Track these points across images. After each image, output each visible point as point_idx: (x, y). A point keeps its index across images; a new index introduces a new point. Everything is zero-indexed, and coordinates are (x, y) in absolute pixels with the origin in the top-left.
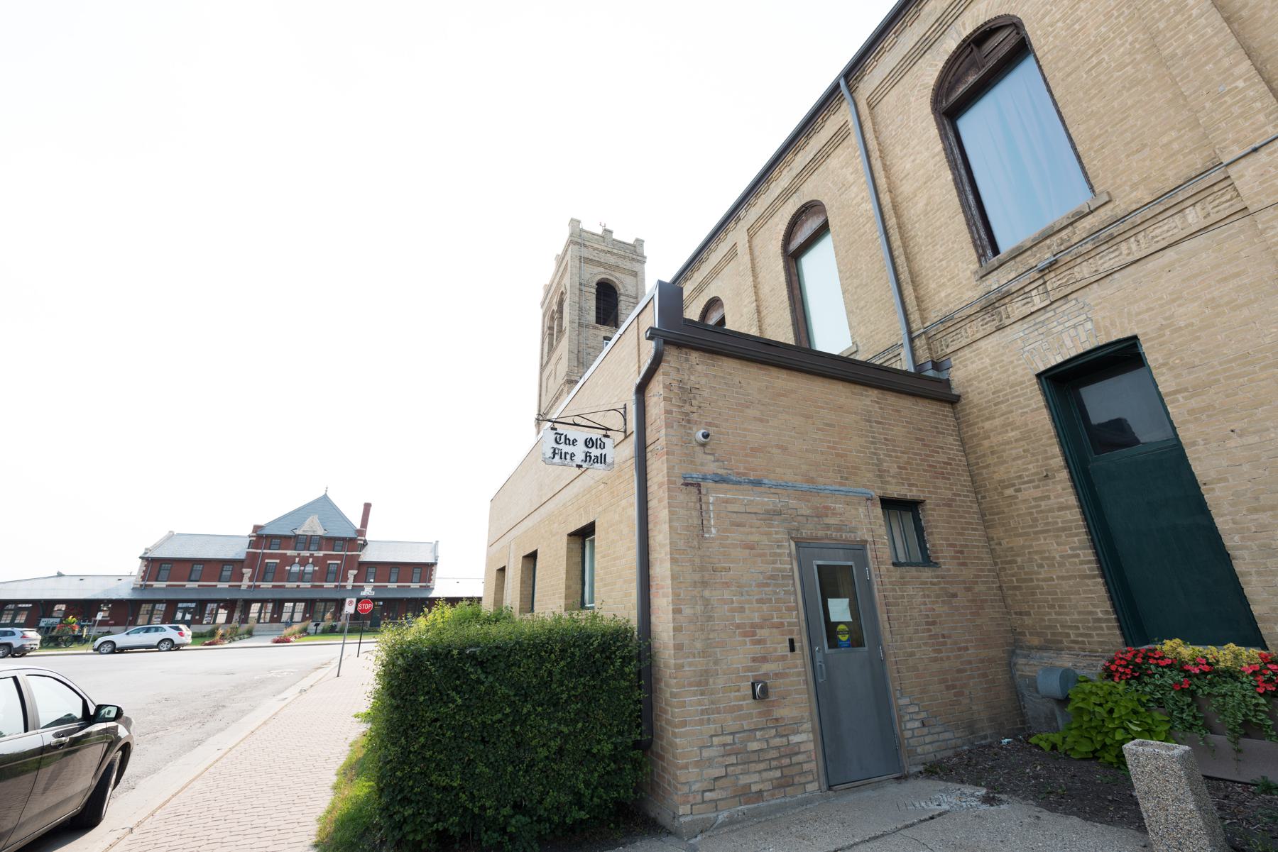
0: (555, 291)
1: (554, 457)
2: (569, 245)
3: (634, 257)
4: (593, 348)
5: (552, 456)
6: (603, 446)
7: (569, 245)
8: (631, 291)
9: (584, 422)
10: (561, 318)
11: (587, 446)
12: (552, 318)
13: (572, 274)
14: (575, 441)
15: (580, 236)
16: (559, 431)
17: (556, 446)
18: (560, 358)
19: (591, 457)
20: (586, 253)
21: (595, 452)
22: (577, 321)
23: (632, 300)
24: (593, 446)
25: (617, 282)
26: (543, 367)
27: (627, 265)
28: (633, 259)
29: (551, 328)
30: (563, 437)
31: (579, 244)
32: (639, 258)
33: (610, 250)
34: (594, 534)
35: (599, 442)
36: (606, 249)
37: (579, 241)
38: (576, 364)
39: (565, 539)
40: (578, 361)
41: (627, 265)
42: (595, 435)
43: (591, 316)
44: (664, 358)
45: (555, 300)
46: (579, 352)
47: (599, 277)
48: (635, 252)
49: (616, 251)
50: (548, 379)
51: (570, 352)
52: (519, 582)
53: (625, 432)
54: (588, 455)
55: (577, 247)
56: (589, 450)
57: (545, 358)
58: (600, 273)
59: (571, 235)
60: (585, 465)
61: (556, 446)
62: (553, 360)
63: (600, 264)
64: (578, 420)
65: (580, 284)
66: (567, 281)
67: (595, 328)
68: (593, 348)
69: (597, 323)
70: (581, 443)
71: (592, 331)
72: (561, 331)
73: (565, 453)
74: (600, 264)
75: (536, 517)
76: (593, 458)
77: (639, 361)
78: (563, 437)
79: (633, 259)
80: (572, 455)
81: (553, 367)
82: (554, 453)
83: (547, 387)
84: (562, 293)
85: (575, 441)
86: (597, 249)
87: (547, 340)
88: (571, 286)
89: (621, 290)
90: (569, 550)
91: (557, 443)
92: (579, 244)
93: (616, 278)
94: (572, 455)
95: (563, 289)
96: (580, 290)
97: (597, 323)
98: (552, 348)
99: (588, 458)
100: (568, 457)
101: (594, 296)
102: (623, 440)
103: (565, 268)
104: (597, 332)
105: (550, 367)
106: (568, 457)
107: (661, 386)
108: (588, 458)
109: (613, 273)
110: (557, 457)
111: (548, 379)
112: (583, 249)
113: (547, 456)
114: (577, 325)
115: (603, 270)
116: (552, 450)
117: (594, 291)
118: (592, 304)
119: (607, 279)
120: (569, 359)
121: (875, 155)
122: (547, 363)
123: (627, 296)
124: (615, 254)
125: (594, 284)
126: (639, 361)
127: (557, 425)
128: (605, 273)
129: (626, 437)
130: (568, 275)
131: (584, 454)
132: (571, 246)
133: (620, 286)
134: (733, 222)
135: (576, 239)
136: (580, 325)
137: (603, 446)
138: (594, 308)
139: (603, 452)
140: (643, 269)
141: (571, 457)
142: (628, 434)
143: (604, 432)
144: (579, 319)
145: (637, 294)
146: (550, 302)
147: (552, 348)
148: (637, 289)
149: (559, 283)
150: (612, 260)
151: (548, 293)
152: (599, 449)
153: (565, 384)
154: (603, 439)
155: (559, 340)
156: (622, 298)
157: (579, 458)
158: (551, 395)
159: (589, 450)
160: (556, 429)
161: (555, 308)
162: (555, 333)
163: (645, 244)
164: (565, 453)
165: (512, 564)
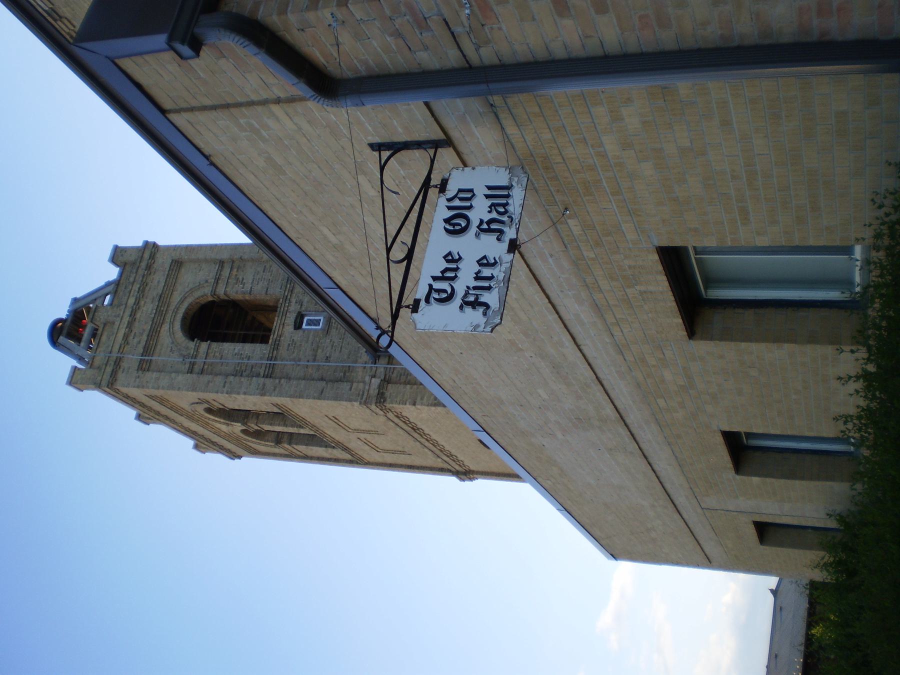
0: (206, 425)
1: (486, 306)
2: (117, 391)
3: (143, 265)
4: (315, 351)
5: (481, 310)
6: (467, 194)
7: (117, 391)
8: (207, 273)
9: (406, 236)
10: (256, 415)
11: (463, 230)
12: (259, 435)
13: (171, 387)
14: (449, 257)
15: (99, 368)
16: (421, 293)
17: (458, 301)
18: (335, 420)
19: (492, 221)
20: (132, 359)
21: (480, 211)
22: (261, 380)
23: (226, 272)
24: (466, 218)
25: (190, 300)
26: (356, 461)
27: (158, 279)
28: (149, 267)
29: (279, 439)
30: (437, 285)
31: (114, 374)
32: (147, 255)
33: (128, 312)
34: (685, 249)
35: (457, 203)
36: (126, 319)
37: (109, 369)
38: (345, 386)
39: (701, 347)
40: (340, 380)
41: (158, 279)
42: (439, 211)
43: (254, 352)
44: (246, 13)
45: (224, 428)
46: (322, 379)
47: (180, 335)
48: (134, 263)
49: (132, 301)
50: (375, 448)
51: (321, 396)
52: (789, 482)
53: (436, 145)
54: (486, 228)
55: (121, 376)
56: (475, 223)
57: (338, 453)
58: (172, 333)
59: (98, 386)
60: (510, 233)
61: (458, 301)
62: (339, 435)
63: (154, 333)
64: (398, 253)
65: (191, 371)
66: (185, 399)
67: (276, 346)
68: (315, 351)
69: (267, 342)
70: (456, 245)
71: (283, 351)
72: (281, 416)
73: (477, 278)
74: (154, 333)
75: (649, 436)
76: (494, 215)
77: (264, 103)
78: (437, 285)
79: (149, 267)
80: (483, 262)
81: (353, 436)
82: (475, 304)
83: (394, 452)
84: (209, 411)
85: (449, 257)
86: (126, 337)
87: (302, 448)
88: (194, 389)
89: (205, 294)
90: (726, 336)
91: (450, 297)
92: (114, 374)
93: (182, 301)
94: (483, 262)
95: (200, 409)
96: (202, 372)
97: (267, 342)
98: (316, 439)
99: (493, 226)
100: (486, 272)
101: (215, 345)
102: (458, 154)
103: (162, 401)
104: (285, 341)
105: (354, 444)
106: (486, 272)
107: (311, 16)
108: (493, 226)
109: (172, 307)
110: (485, 297)
111: (375, 448)
112: (124, 364)
113: (482, 320)
114: (268, 381)
115: (166, 327)
116: (468, 310)
117: (204, 346)
118: (230, 349)
119: (184, 319)
120: (336, 398)
121: (369, 443)
122: (346, 449)
123: (217, 280)
124: (137, 302)
125: (192, 345)
126: (264, 103)
127: (408, 300)
128: (172, 323)
129: (448, 142)
130: (172, 396)
131: (483, 236)
132: (118, 386)
133: (198, 294)
134: (59, 25)
135: (106, 377)
136: (269, 374)
137: (467, 194)
138: (237, 347)
139: (481, 191)
140: (169, 248)
141: (488, 265)
142: (442, 136)
143: (433, 193)
144: (258, 375)
145: (214, 261)
146: (228, 437)
147: (316, 439)
148: (206, 261)
149: (191, 417)
150: (148, 308)
151: (214, 443)
152: (474, 202)
153: (385, 410)
154: (450, 193)
155: (301, 422)
156: (221, 291)
157: (491, 246)
158: (409, 444)
159: (475, 223)
160: (417, 302)
161: (238, 427)
162: (285, 429)
163: (121, 244)
164: (477, 278)
165: (744, 503)
